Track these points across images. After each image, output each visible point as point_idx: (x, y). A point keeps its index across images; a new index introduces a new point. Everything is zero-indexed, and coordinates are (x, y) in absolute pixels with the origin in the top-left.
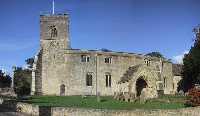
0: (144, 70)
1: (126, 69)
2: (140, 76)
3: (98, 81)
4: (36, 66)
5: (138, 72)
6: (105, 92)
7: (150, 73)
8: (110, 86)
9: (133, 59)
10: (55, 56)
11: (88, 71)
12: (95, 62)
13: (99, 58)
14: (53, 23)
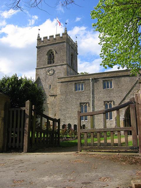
11: (83, 102)
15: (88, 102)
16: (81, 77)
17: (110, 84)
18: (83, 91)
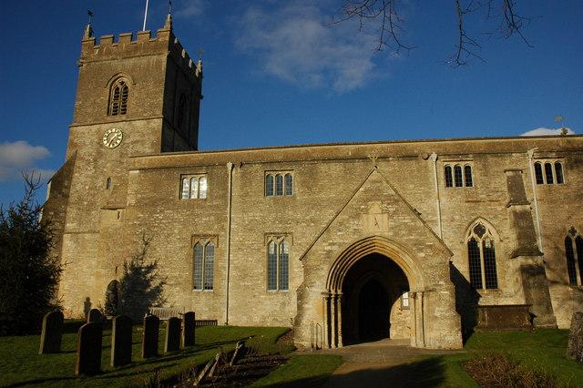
0: (376, 207)
3: (236, 268)
5: (341, 224)
6: (263, 313)
7: (408, 219)
12: (224, 196)
13: (243, 175)
14: (117, 64)
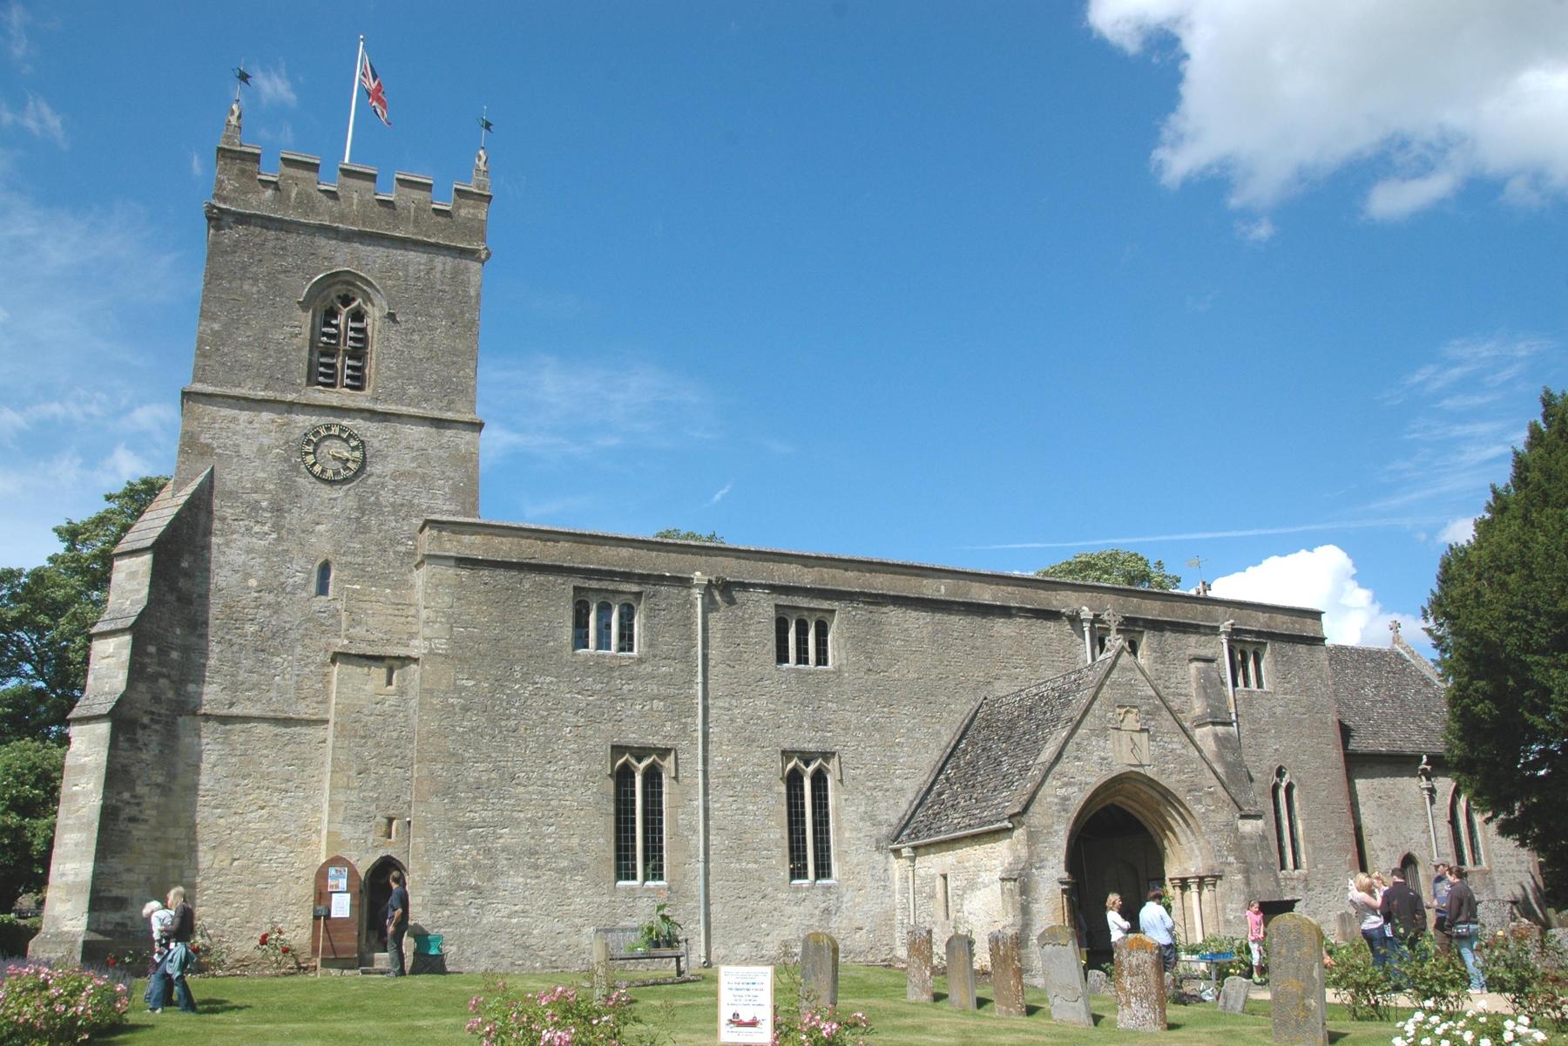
1: (961, 709)
2: (1095, 779)
4: (126, 654)
8: (823, 870)
9: (1003, 628)
10: (325, 569)
11: (632, 738)
15: (670, 744)
16: (625, 552)
17: (599, 619)
18: (640, 661)
